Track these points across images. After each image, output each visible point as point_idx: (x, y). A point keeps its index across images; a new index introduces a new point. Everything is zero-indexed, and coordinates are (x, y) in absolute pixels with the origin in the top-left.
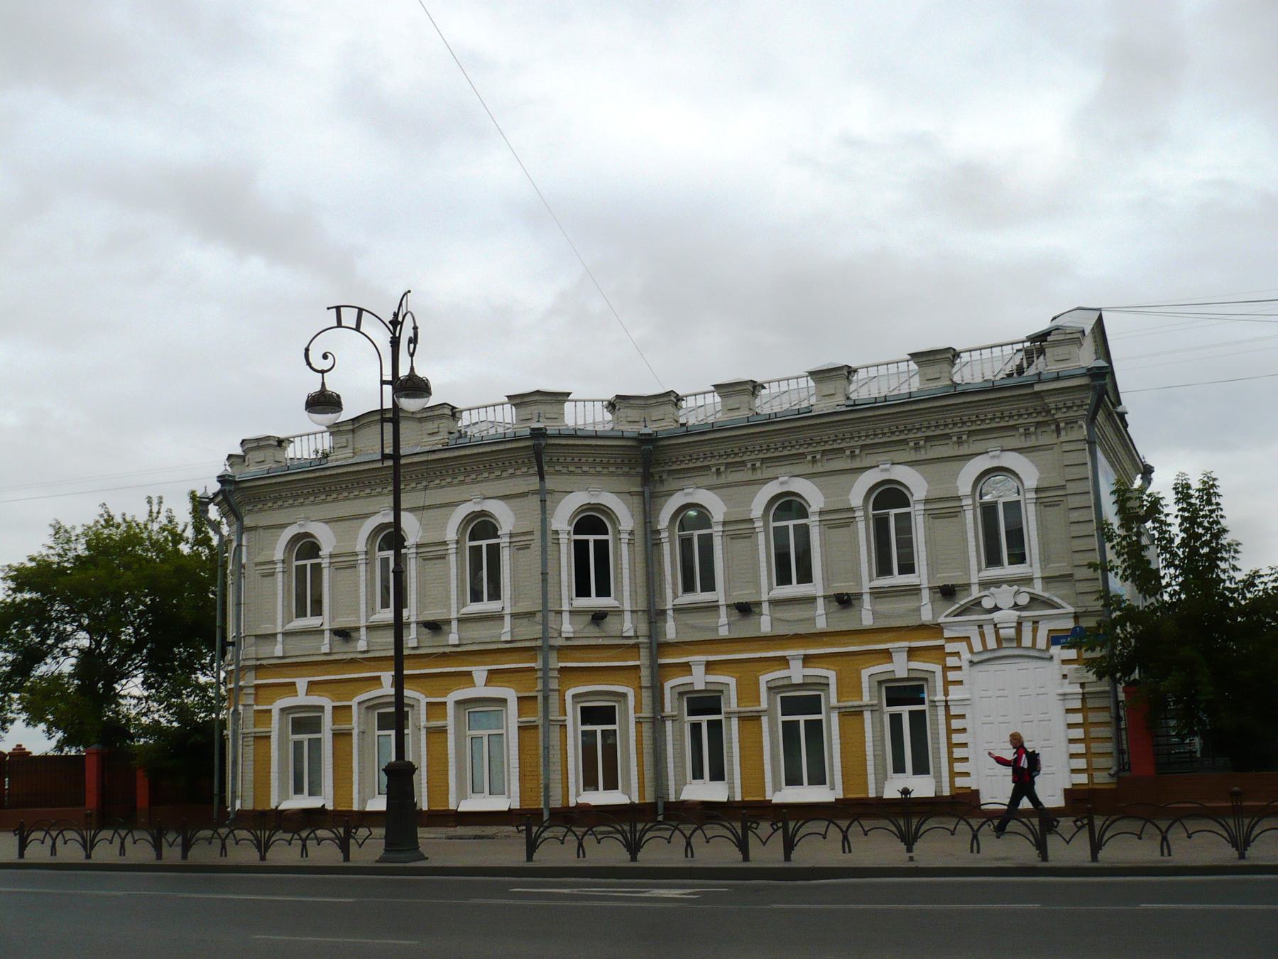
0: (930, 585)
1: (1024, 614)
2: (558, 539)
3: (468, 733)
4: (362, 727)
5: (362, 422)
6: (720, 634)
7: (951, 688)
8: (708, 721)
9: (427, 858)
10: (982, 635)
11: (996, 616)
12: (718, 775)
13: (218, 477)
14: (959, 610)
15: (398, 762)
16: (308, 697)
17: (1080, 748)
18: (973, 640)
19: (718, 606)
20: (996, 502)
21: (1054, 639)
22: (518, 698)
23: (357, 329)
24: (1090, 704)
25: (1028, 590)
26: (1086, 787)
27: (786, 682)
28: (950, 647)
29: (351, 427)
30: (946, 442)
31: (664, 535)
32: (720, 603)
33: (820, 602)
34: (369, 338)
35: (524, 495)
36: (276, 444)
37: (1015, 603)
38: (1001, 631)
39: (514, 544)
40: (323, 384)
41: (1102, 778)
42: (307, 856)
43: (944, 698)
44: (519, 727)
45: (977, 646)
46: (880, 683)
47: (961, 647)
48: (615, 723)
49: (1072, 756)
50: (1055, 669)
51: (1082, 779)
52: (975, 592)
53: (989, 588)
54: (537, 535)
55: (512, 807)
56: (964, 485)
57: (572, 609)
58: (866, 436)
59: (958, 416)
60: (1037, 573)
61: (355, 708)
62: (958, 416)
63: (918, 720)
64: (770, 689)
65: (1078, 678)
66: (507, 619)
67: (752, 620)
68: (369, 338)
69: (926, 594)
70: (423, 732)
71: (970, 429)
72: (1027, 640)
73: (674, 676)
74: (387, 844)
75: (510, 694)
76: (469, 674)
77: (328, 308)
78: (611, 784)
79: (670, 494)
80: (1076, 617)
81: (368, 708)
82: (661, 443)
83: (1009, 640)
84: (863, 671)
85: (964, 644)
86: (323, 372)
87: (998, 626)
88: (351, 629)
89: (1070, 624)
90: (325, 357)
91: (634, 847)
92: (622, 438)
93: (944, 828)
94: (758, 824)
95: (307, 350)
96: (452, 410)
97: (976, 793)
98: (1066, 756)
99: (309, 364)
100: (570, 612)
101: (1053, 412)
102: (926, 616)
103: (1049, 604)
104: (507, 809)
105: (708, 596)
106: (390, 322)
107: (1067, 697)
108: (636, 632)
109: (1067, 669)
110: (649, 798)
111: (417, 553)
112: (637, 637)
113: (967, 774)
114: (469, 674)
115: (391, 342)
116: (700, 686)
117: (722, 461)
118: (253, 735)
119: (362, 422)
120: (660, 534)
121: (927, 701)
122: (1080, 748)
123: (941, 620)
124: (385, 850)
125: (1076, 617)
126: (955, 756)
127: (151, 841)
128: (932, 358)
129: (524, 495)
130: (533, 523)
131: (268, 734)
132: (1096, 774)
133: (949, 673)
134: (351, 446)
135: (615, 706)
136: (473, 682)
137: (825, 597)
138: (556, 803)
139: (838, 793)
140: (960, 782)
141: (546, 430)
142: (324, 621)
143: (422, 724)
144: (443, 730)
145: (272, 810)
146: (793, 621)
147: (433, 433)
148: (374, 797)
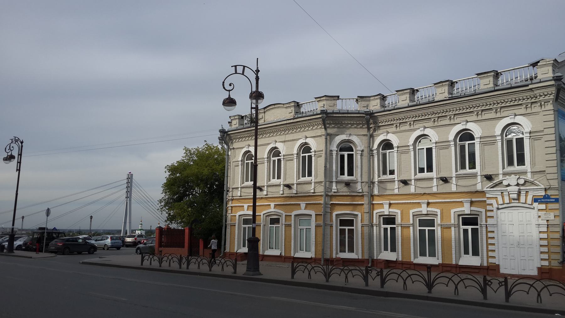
0: (481, 174)
1: (522, 188)
2: (332, 153)
3: (299, 227)
4: (264, 223)
5: (275, 106)
6: (453, 190)
7: (488, 219)
8: (390, 227)
9: (262, 275)
10: (503, 197)
11: (509, 189)
12: (393, 249)
13: (219, 130)
14: (493, 185)
15: (253, 237)
16: (248, 211)
17: (545, 249)
18: (499, 199)
19: (395, 181)
20: (513, 138)
21: (535, 200)
22: (316, 215)
23: (243, 74)
24: (551, 229)
25: (523, 177)
26: (548, 267)
27: (420, 213)
28: (489, 201)
29: (263, 111)
30: (491, 112)
31: (375, 152)
32: (396, 180)
33: (435, 180)
34: (225, 80)
35: (320, 136)
36: (241, 118)
37: (518, 183)
38: (511, 195)
39: (285, 159)
40: (229, 95)
41: (555, 264)
42: (223, 271)
43: (485, 224)
44: (316, 226)
45: (500, 202)
46: (459, 215)
47: (493, 202)
48: (353, 226)
49: (541, 253)
50: (534, 213)
51: (546, 263)
52: (501, 177)
53: (506, 176)
54: (324, 152)
55: (312, 257)
56: (498, 131)
57: (337, 181)
58: (456, 110)
59: (495, 101)
60: (529, 170)
61: (293, 217)
62: (495, 101)
63: (475, 232)
64: (414, 216)
65: (546, 218)
66: (313, 183)
67: (407, 187)
68: (225, 80)
69: (479, 178)
70: (284, 226)
71: (501, 106)
72: (522, 199)
73: (377, 209)
74: (247, 268)
75: (313, 213)
76: (299, 205)
77: (232, 67)
78: (351, 250)
79: (379, 135)
80: (546, 190)
81: (267, 216)
82: (376, 115)
83: (514, 199)
84: (410, 211)
85: (495, 200)
86: (229, 91)
87: (510, 193)
88: (262, 186)
89: (543, 193)
90: (230, 85)
91: (327, 275)
92: (359, 113)
93: (495, 279)
94: (372, 271)
95: (223, 82)
96: (297, 104)
97: (498, 266)
98: (539, 252)
99: (224, 88)
100: (336, 182)
101: (538, 97)
102: (479, 187)
103: (532, 183)
104: (310, 257)
105: (521, 168)
106: (256, 71)
107: (540, 226)
108: (362, 190)
109: (540, 213)
110: (366, 257)
111: (436, 146)
112: (363, 192)
113: (494, 257)
114: (299, 205)
115: (256, 78)
116: (387, 213)
117: (398, 122)
118: (230, 224)
119: (275, 106)
120: (333, 151)
121: (479, 225)
122: (545, 249)
123: (485, 189)
124: (247, 271)
125: (546, 190)
126: (489, 249)
127: (158, 260)
128: (486, 75)
129: (320, 136)
130: (323, 147)
131: (235, 224)
132: (553, 262)
133: (488, 213)
134: (263, 119)
135: (353, 220)
136: (301, 208)
137: (437, 178)
138: (328, 257)
139: (440, 261)
140: (491, 260)
141: (327, 111)
142: (281, 181)
143: (283, 223)
144: (290, 226)
145: (235, 252)
146: (423, 187)
147: (290, 113)
148: (267, 250)
